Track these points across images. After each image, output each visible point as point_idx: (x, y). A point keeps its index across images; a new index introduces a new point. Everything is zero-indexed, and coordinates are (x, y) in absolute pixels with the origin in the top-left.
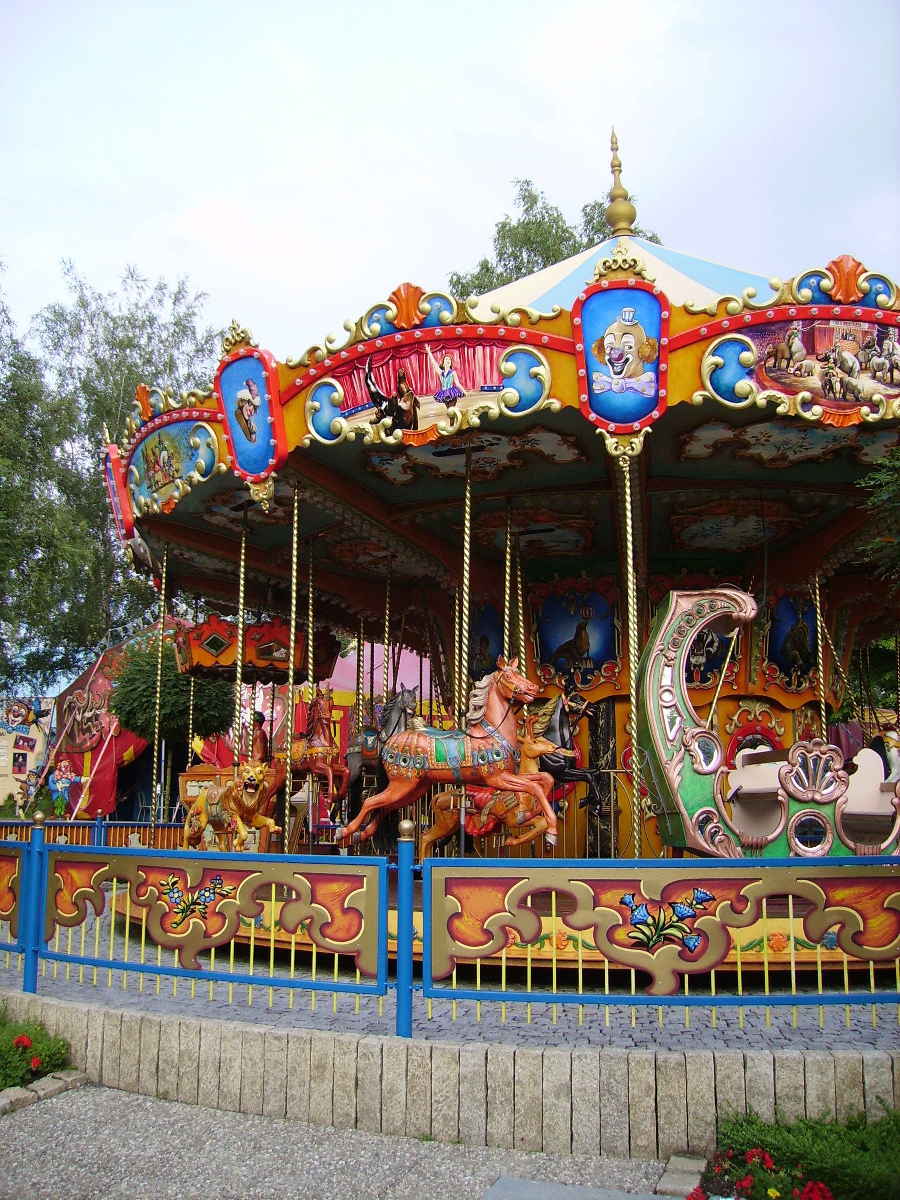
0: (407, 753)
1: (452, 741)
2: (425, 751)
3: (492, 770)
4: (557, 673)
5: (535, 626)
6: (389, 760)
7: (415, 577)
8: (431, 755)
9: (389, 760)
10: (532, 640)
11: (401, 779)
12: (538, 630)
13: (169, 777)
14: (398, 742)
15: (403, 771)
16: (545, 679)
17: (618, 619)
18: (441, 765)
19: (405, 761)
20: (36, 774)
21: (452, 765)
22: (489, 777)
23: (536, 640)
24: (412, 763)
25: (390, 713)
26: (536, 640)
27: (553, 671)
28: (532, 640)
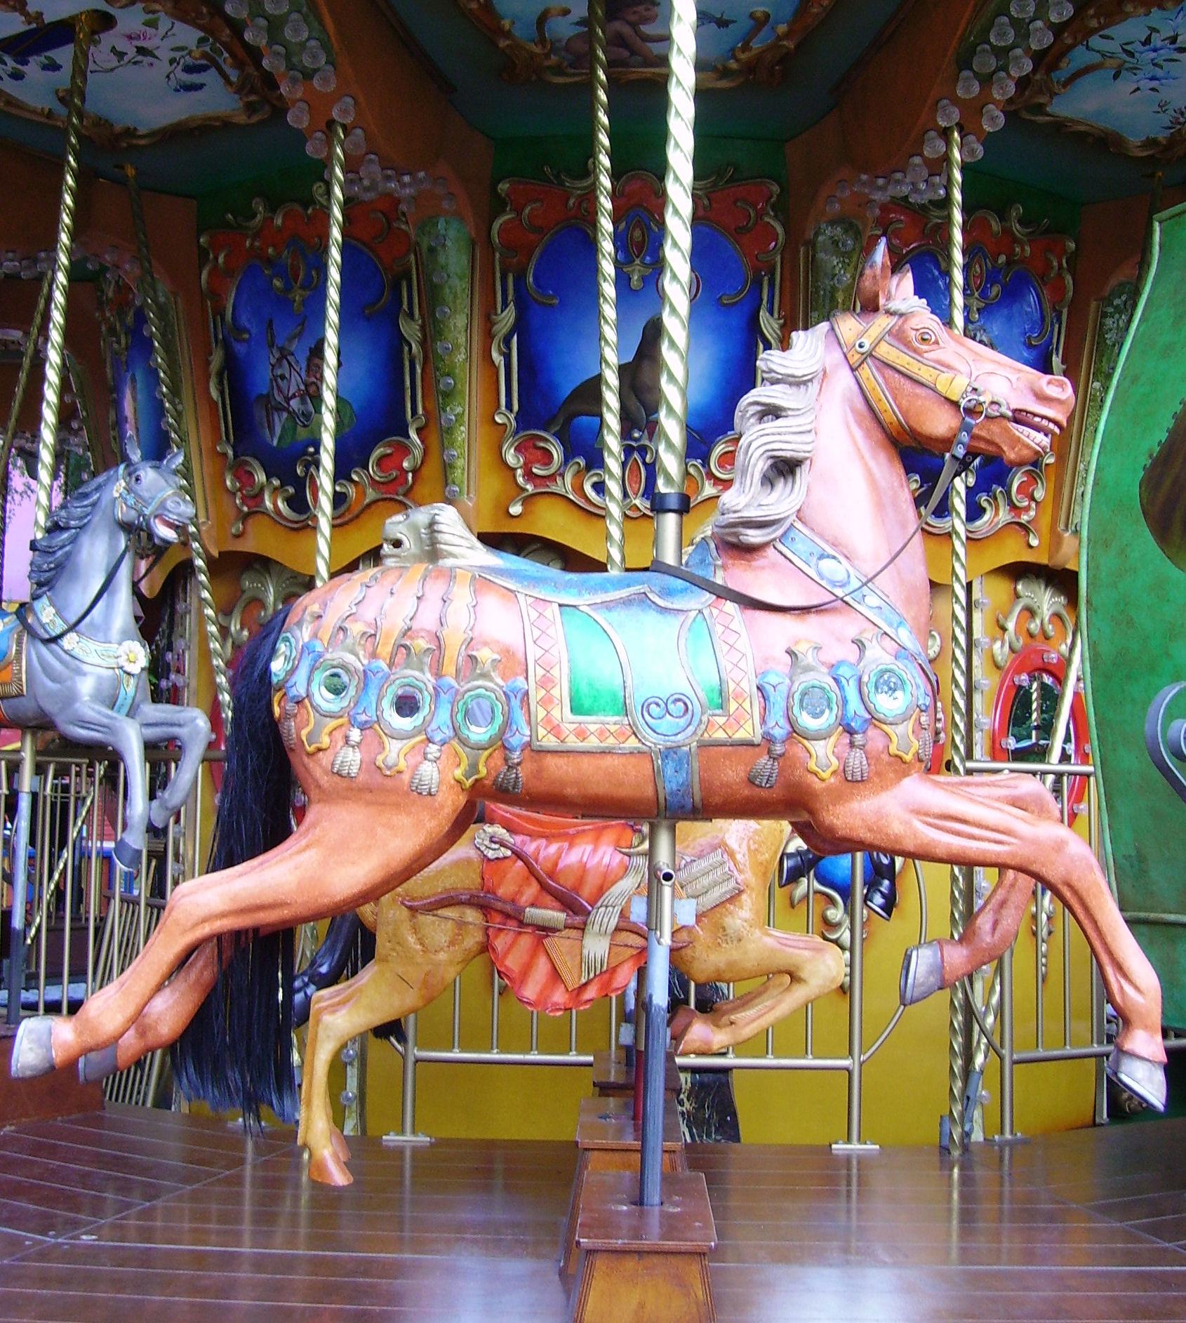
0: (414, 678)
1: (650, 619)
2: (512, 662)
3: (857, 760)
4: (567, 459)
5: (507, 318)
6: (323, 699)
7: (130, 133)
8: (546, 682)
9: (323, 699)
10: (497, 358)
11: (381, 790)
12: (520, 326)
13: (474, 393)
14: (369, 612)
15: (394, 752)
16: (529, 475)
17: (771, 313)
18: (599, 730)
19: (406, 705)
20: (943, 979)
21: (667, 730)
22: (838, 797)
23: (508, 358)
24: (443, 715)
25: (74, 540)
26: (508, 358)
27: (557, 453)
28: (497, 358)
